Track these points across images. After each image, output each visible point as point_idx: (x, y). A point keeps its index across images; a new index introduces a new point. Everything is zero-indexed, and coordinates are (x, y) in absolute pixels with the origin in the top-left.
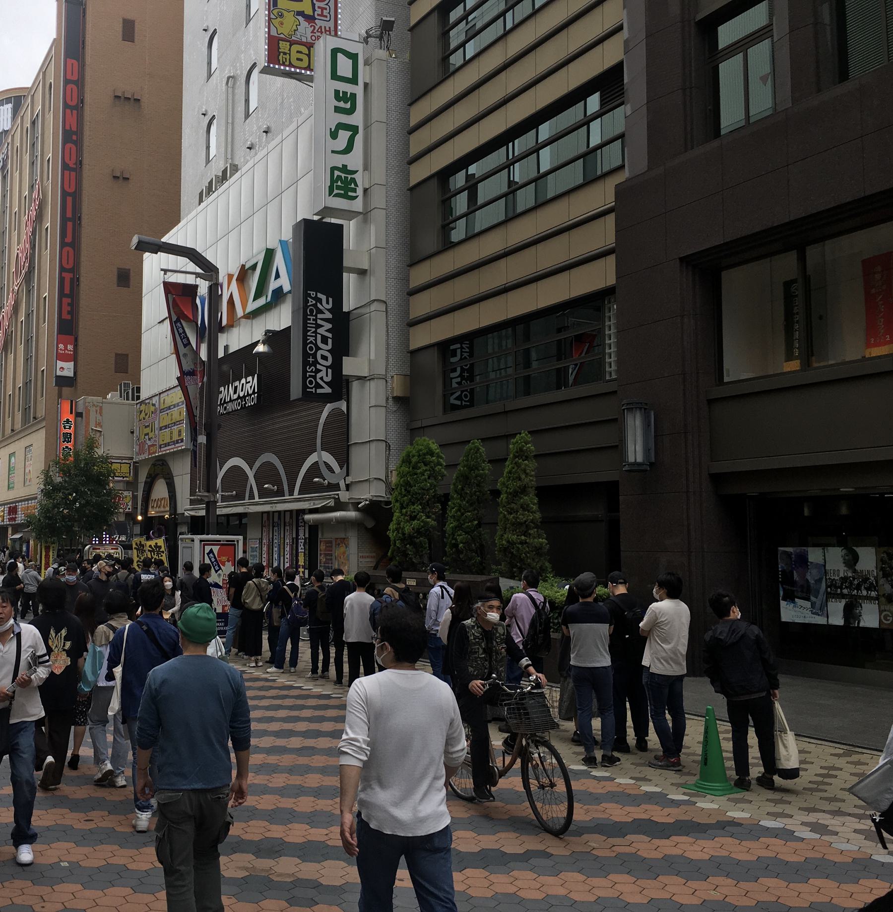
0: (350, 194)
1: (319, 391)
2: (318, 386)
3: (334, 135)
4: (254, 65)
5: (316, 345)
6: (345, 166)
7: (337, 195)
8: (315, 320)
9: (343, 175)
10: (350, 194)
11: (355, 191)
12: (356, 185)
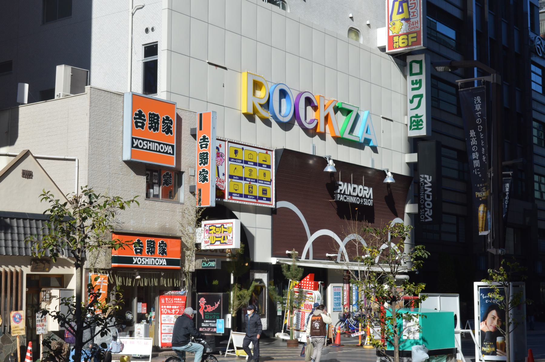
0: (420, 127)
1: (426, 220)
2: (426, 218)
3: (411, 102)
4: (201, 129)
5: (424, 199)
6: (417, 115)
7: (413, 129)
8: (424, 188)
9: (416, 119)
10: (420, 127)
11: (422, 125)
12: (422, 122)
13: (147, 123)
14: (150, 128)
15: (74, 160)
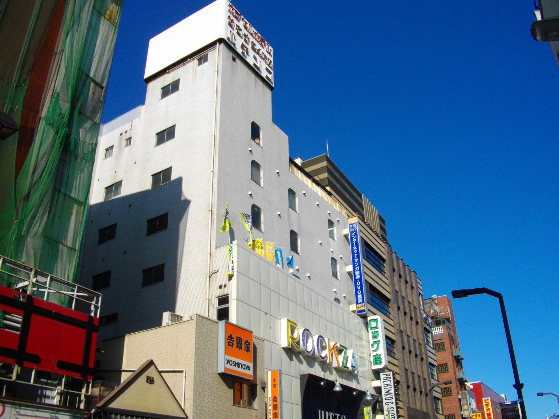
3: (372, 345)
7: (276, 252)
13: (235, 343)
14: (237, 347)
15: (182, 372)
